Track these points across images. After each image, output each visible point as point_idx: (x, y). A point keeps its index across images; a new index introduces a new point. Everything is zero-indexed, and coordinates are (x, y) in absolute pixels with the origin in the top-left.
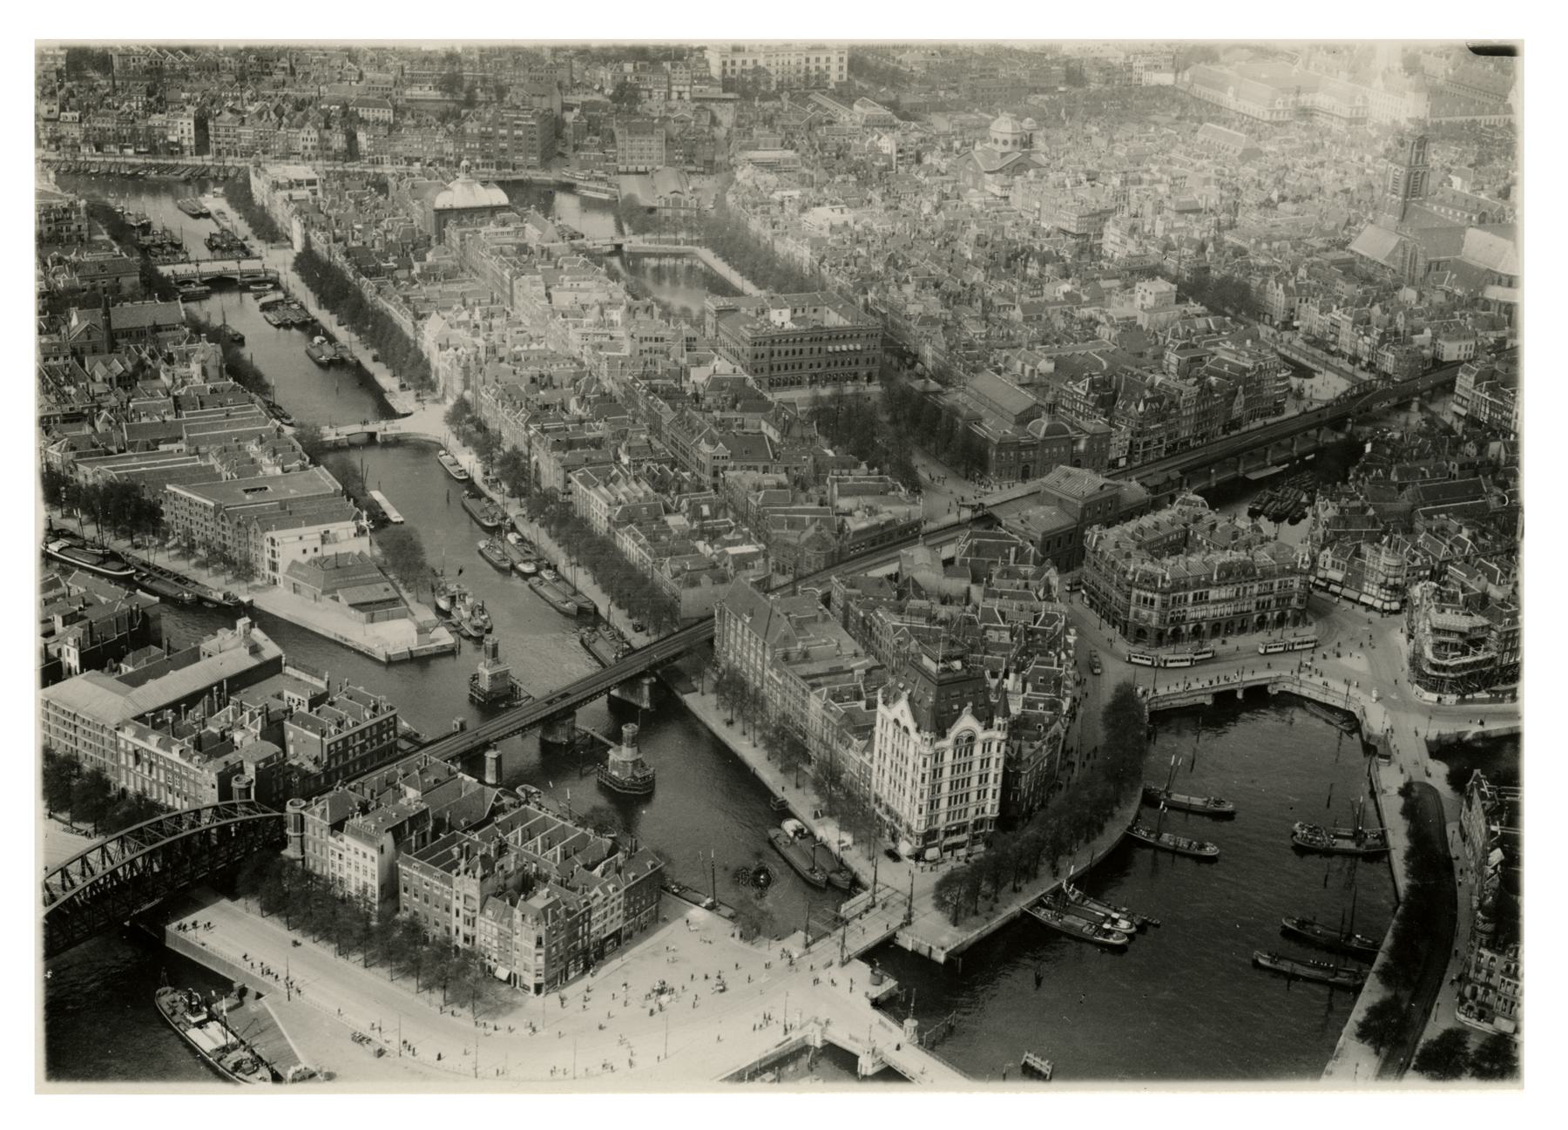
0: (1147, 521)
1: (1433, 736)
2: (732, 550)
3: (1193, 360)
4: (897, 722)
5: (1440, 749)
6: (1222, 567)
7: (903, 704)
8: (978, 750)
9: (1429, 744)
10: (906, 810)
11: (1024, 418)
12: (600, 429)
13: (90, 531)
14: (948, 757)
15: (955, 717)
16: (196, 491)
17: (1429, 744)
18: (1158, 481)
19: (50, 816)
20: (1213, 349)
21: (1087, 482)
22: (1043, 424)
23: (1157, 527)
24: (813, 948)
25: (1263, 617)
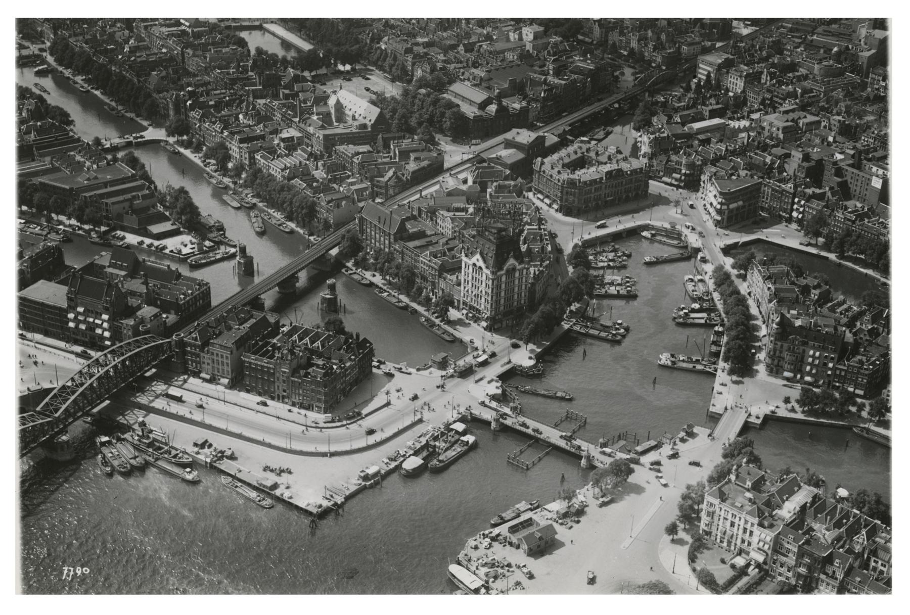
0: (563, 152)
1: (722, 246)
2: (353, 188)
3: (560, 66)
4: (474, 265)
5: (727, 251)
6: (607, 173)
7: (478, 256)
8: (517, 274)
9: (722, 249)
10: (483, 306)
11: (483, 106)
12: (259, 130)
13: (523, 295)
14: (504, 279)
15: (505, 261)
16: (63, 183)
17: (722, 249)
18: (560, 131)
19: (22, 337)
20: (571, 60)
21: (525, 136)
22: (493, 108)
23: (569, 155)
24: (715, 435)
25: (627, 196)
